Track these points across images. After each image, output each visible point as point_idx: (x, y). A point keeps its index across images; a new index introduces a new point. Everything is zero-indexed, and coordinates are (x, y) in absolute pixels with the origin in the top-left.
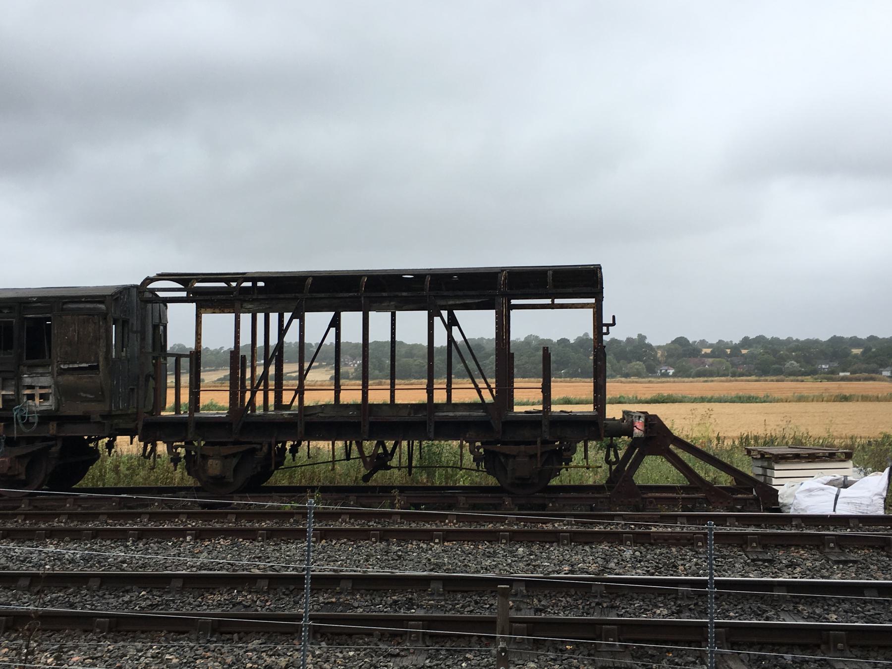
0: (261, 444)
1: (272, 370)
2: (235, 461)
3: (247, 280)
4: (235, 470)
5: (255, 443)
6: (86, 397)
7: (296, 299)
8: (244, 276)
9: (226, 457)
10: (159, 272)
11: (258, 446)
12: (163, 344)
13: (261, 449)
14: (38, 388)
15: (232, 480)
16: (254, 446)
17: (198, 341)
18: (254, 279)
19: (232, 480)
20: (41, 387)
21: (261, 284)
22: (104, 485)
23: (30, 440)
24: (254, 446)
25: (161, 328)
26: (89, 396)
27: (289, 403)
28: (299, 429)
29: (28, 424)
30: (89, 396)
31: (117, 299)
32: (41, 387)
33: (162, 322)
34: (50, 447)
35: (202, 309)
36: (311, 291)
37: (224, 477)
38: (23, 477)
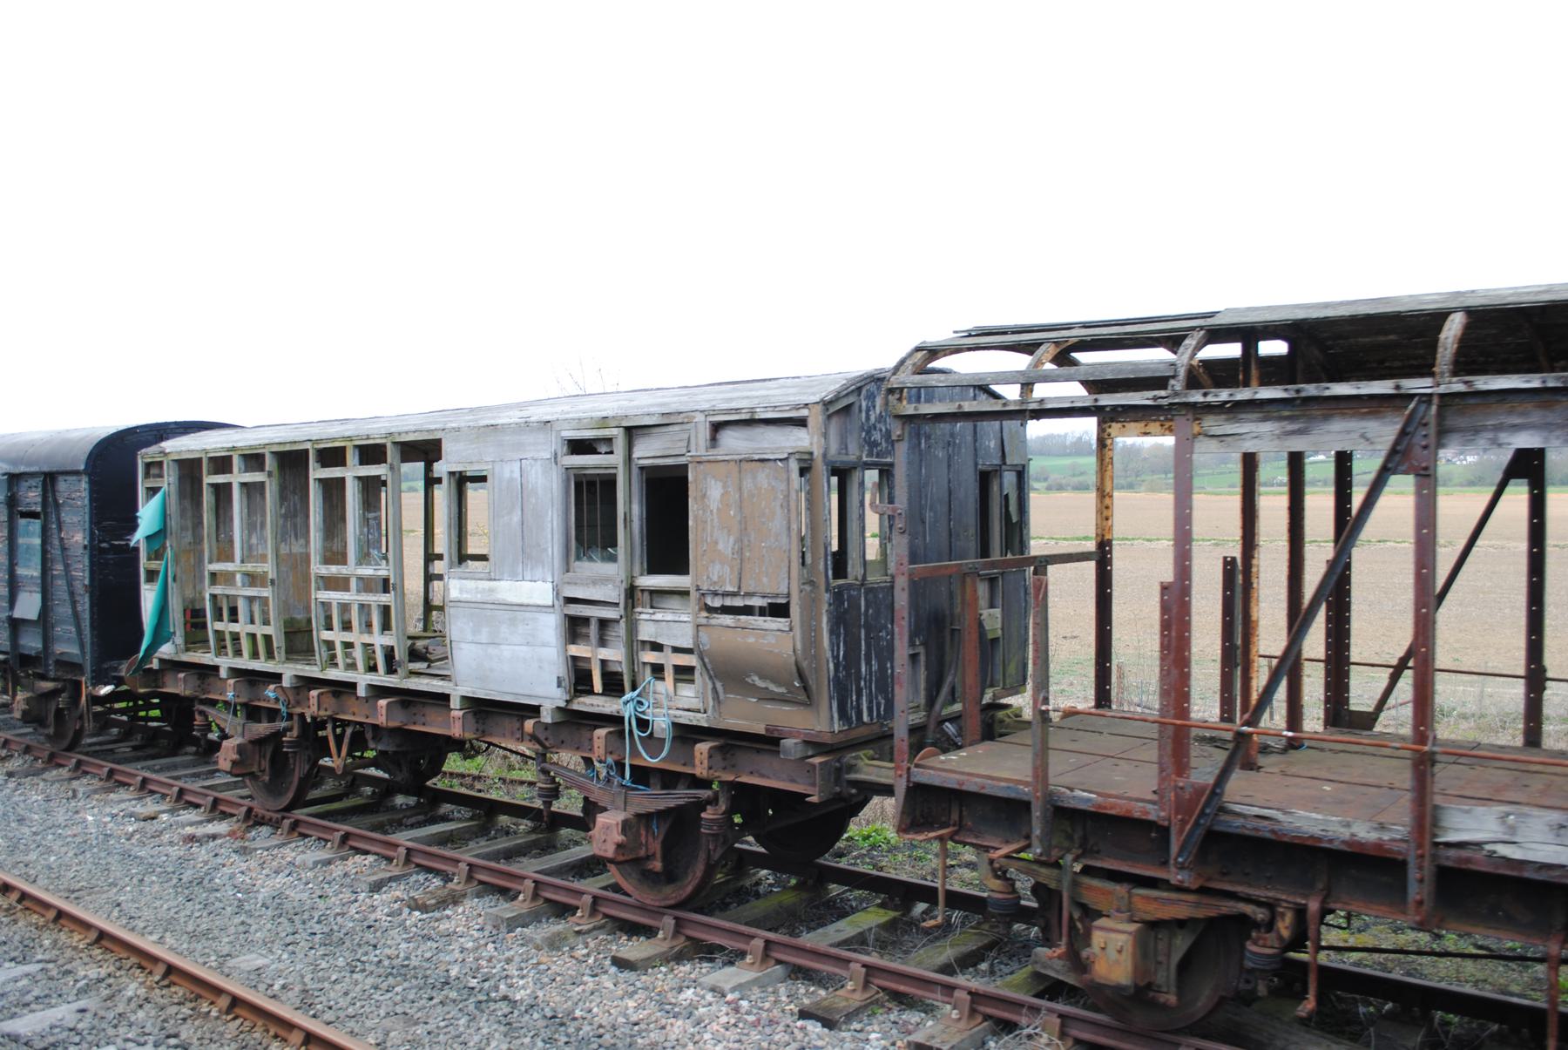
0: (1270, 906)
1: (1315, 643)
2: (1182, 943)
3: (1218, 334)
4: (1185, 966)
5: (1248, 900)
6: (767, 688)
7: (1396, 401)
8: (1210, 322)
9: (1154, 926)
10: (969, 325)
11: (1260, 914)
12: (1015, 519)
13: (1270, 925)
14: (670, 650)
15: (1172, 999)
16: (1248, 909)
17: (1105, 513)
18: (1248, 334)
19: (1172, 999)
20: (676, 650)
21: (1274, 348)
22: (1358, 459)
23: (669, 779)
24: (1248, 909)
25: (1009, 478)
26: (773, 687)
27: (1512, 481)
28: (1414, 891)
29: (653, 742)
30: (773, 687)
31: (847, 409)
32: (676, 650)
33: (1008, 462)
34: (701, 805)
35: (1114, 424)
36: (1467, 362)
37: (1149, 986)
38: (657, 865)
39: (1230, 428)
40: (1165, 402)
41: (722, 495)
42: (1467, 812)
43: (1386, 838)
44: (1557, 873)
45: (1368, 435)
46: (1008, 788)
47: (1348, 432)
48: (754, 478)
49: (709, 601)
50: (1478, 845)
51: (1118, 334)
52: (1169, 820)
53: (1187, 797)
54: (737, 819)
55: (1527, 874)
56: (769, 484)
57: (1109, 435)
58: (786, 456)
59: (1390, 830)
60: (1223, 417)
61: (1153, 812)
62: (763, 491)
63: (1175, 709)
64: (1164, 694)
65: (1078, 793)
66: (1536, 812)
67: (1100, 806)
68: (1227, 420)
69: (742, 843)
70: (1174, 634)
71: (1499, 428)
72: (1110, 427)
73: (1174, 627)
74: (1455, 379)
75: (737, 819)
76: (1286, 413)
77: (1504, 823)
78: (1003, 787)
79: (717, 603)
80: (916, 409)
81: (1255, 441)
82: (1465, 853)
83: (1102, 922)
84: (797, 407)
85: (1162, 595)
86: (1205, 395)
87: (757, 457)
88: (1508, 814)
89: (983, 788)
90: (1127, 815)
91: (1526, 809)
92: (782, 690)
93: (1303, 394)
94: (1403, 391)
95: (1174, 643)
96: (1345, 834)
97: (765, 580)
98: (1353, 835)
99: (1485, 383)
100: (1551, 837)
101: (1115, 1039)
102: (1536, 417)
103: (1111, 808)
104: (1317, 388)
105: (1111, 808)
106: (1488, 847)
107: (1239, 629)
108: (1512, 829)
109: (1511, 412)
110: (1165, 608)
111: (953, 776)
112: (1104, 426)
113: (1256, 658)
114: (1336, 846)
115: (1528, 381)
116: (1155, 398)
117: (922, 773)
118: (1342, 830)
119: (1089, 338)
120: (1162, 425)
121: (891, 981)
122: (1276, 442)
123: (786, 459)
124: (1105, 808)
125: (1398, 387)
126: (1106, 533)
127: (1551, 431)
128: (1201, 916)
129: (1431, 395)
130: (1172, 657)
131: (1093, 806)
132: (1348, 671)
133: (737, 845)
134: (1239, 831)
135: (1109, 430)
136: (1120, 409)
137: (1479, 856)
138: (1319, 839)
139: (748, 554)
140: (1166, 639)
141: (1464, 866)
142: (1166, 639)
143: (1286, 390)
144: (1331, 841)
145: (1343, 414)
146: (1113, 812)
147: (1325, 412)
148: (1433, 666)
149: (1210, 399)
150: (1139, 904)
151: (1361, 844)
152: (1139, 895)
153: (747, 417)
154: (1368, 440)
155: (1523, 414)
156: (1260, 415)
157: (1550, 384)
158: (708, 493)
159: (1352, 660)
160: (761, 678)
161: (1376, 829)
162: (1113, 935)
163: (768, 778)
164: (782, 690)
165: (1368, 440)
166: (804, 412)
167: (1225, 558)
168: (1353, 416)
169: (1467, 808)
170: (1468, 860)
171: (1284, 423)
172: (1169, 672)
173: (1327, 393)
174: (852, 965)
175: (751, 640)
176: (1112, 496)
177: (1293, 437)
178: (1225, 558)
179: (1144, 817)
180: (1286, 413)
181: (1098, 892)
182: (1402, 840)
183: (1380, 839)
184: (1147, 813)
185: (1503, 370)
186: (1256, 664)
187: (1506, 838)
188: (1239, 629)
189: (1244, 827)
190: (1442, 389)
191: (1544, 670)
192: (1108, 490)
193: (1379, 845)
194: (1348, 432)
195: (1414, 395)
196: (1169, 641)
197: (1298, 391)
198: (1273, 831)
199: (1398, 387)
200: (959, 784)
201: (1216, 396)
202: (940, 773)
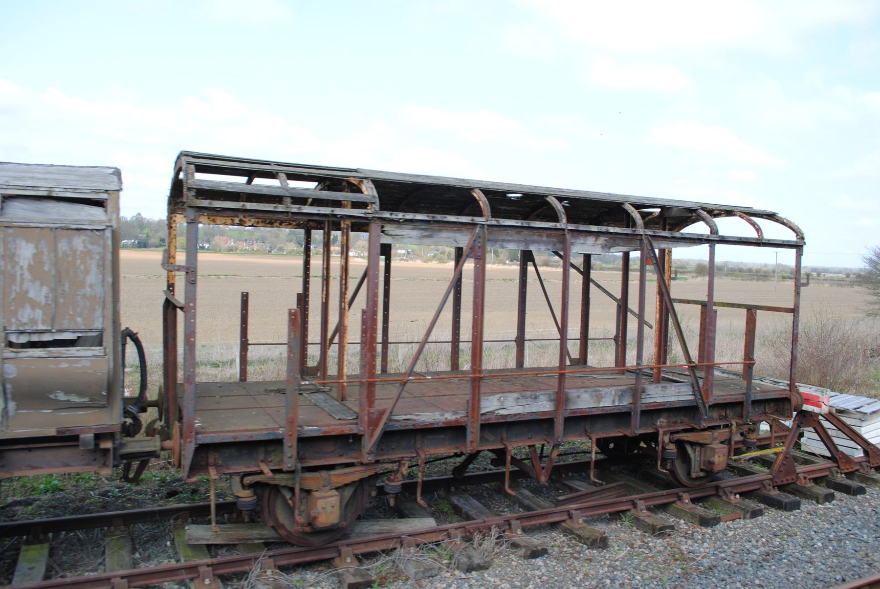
0: (399, 462)
39: (398, 232)
40: (370, 216)
41: (34, 255)
42: (487, 400)
43: (459, 417)
44: (518, 417)
45: (457, 240)
46: (269, 433)
47: (449, 238)
48: (70, 242)
49: (13, 338)
50: (492, 412)
51: (323, 174)
52: (365, 431)
53: (375, 417)
54: (611, 446)
55: (508, 420)
56: (85, 247)
57: (174, 221)
58: (104, 227)
59: (459, 413)
60: (395, 226)
61: (355, 428)
62: (78, 253)
63: (368, 374)
64: (363, 366)
65: (306, 428)
66: (509, 395)
67: (326, 432)
68: (397, 228)
69: (468, 472)
70: (368, 335)
71: (503, 241)
72: (175, 216)
73: (369, 332)
74: (493, 219)
75: (611, 446)
76: (423, 227)
77: (500, 401)
78: (266, 434)
79: (23, 339)
80: (210, 204)
81: (409, 239)
82: (487, 417)
83: (316, 494)
84: (97, 192)
85: (363, 316)
86: (391, 214)
87: (74, 227)
88: (501, 397)
89: (252, 437)
90: (342, 433)
91: (506, 394)
92: (86, 399)
93: (436, 219)
94: (475, 222)
95: (368, 340)
96: (442, 419)
97: (79, 319)
98: (446, 419)
99: (503, 222)
100: (515, 404)
101: (301, 557)
102: (516, 237)
103: (333, 431)
104: (441, 217)
105: (333, 431)
106: (496, 412)
107: (663, 330)
108: (503, 403)
109: (507, 234)
110: (364, 322)
111: (230, 434)
112: (172, 215)
113: (346, 345)
114: (441, 425)
115: (517, 223)
116: (365, 213)
117: (206, 437)
118: (441, 418)
119: (306, 174)
120: (209, 218)
121: (141, 581)
122: (419, 240)
123: (103, 230)
124: (329, 432)
125: (473, 220)
126: (170, 279)
127: (520, 243)
128: (366, 476)
129: (483, 225)
130: (367, 347)
131: (322, 433)
132: (307, 348)
133: (466, 475)
134: (398, 429)
135: (174, 218)
136: (345, 217)
137: (492, 416)
138: (433, 424)
139: (61, 300)
140: (365, 338)
141: (487, 422)
142: (365, 338)
143: (428, 216)
144: (438, 424)
145: (447, 230)
146: (333, 434)
147: (440, 228)
148: (566, 337)
149: (393, 216)
150: (334, 479)
151: (450, 422)
152: (334, 475)
153: (45, 194)
154: (456, 242)
155: (511, 236)
156: (412, 227)
157: (524, 225)
158: (18, 252)
159: (309, 342)
160: (67, 393)
161: (453, 414)
162: (329, 499)
163: (41, 468)
164: (86, 399)
165: (456, 242)
166: (104, 196)
167: (243, 293)
168: (451, 231)
169: (486, 398)
170: (489, 419)
171: (423, 231)
172: (365, 355)
173: (445, 220)
174: (113, 580)
175: (65, 365)
176: (174, 258)
177: (426, 238)
178: (243, 293)
179: (351, 432)
180: (423, 227)
181: (311, 480)
182: (464, 417)
183: (457, 418)
184: (352, 430)
185: (510, 218)
186: (346, 348)
187: (502, 407)
188: (663, 330)
189: (401, 426)
190: (489, 223)
191: (248, 340)
192: (172, 254)
193: (456, 421)
194: (449, 238)
195: (478, 224)
196: (366, 339)
197: (433, 217)
198: (414, 425)
199: (473, 220)
200: (235, 439)
201: (397, 215)
202: (219, 434)
